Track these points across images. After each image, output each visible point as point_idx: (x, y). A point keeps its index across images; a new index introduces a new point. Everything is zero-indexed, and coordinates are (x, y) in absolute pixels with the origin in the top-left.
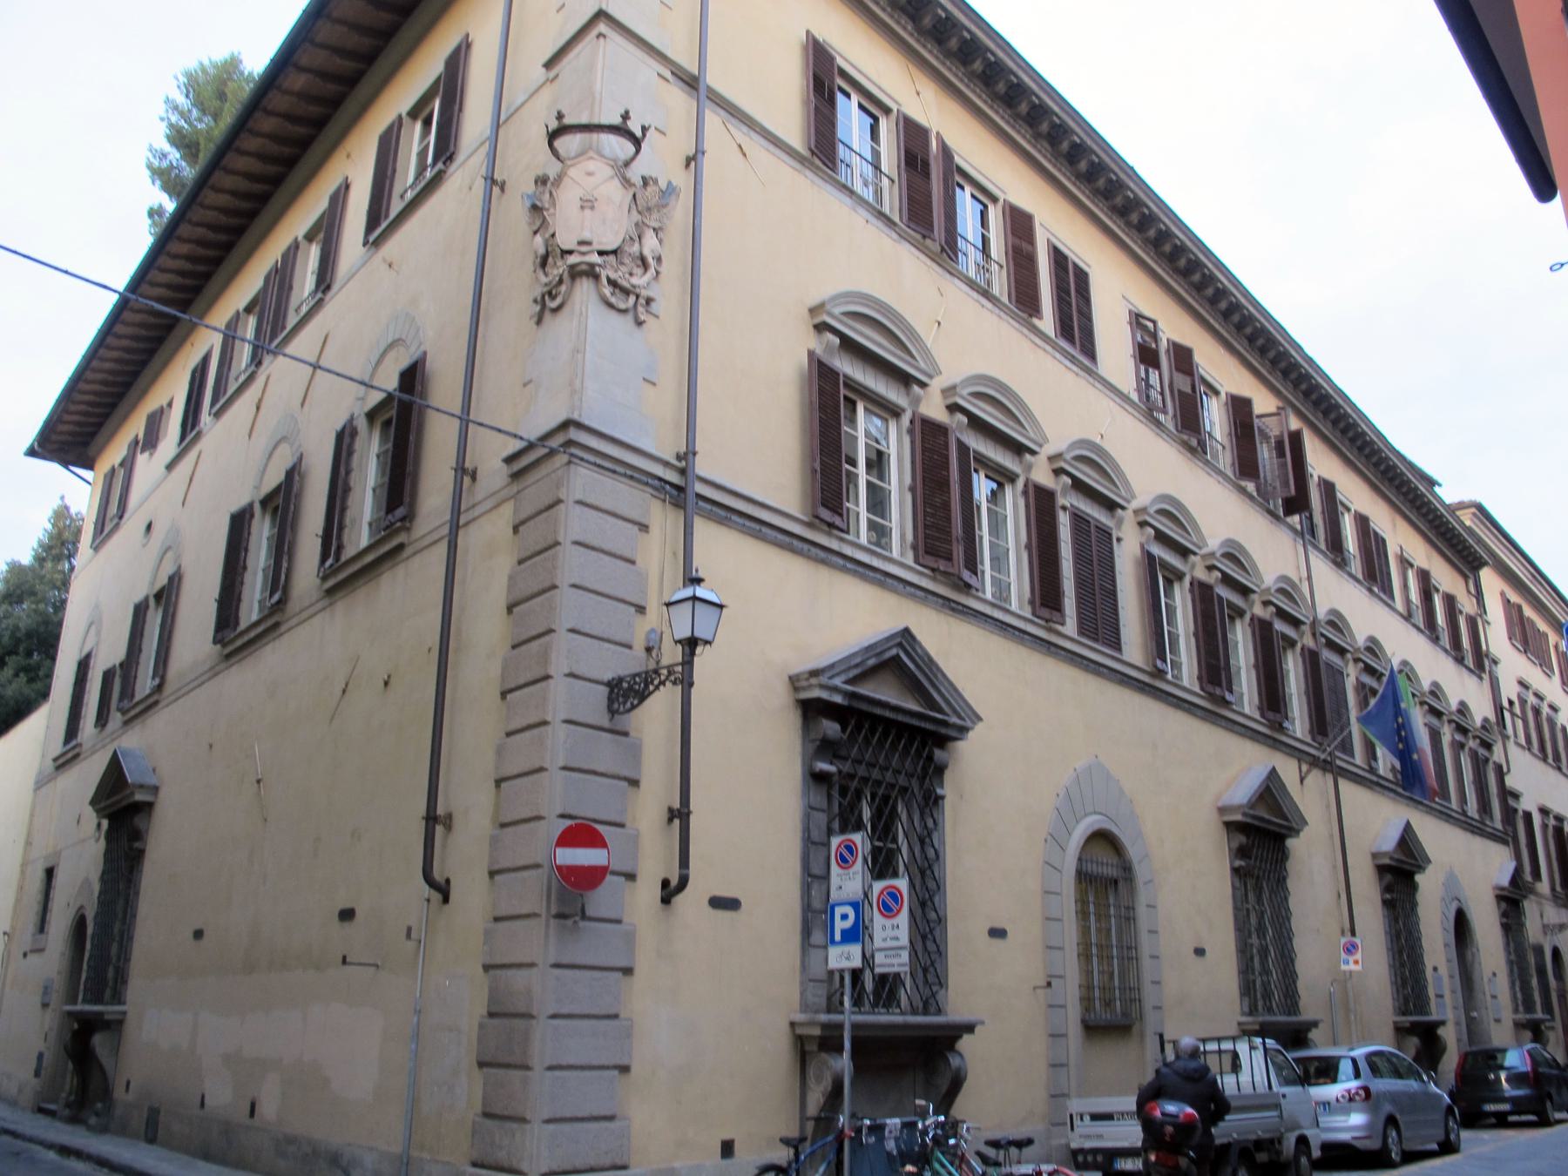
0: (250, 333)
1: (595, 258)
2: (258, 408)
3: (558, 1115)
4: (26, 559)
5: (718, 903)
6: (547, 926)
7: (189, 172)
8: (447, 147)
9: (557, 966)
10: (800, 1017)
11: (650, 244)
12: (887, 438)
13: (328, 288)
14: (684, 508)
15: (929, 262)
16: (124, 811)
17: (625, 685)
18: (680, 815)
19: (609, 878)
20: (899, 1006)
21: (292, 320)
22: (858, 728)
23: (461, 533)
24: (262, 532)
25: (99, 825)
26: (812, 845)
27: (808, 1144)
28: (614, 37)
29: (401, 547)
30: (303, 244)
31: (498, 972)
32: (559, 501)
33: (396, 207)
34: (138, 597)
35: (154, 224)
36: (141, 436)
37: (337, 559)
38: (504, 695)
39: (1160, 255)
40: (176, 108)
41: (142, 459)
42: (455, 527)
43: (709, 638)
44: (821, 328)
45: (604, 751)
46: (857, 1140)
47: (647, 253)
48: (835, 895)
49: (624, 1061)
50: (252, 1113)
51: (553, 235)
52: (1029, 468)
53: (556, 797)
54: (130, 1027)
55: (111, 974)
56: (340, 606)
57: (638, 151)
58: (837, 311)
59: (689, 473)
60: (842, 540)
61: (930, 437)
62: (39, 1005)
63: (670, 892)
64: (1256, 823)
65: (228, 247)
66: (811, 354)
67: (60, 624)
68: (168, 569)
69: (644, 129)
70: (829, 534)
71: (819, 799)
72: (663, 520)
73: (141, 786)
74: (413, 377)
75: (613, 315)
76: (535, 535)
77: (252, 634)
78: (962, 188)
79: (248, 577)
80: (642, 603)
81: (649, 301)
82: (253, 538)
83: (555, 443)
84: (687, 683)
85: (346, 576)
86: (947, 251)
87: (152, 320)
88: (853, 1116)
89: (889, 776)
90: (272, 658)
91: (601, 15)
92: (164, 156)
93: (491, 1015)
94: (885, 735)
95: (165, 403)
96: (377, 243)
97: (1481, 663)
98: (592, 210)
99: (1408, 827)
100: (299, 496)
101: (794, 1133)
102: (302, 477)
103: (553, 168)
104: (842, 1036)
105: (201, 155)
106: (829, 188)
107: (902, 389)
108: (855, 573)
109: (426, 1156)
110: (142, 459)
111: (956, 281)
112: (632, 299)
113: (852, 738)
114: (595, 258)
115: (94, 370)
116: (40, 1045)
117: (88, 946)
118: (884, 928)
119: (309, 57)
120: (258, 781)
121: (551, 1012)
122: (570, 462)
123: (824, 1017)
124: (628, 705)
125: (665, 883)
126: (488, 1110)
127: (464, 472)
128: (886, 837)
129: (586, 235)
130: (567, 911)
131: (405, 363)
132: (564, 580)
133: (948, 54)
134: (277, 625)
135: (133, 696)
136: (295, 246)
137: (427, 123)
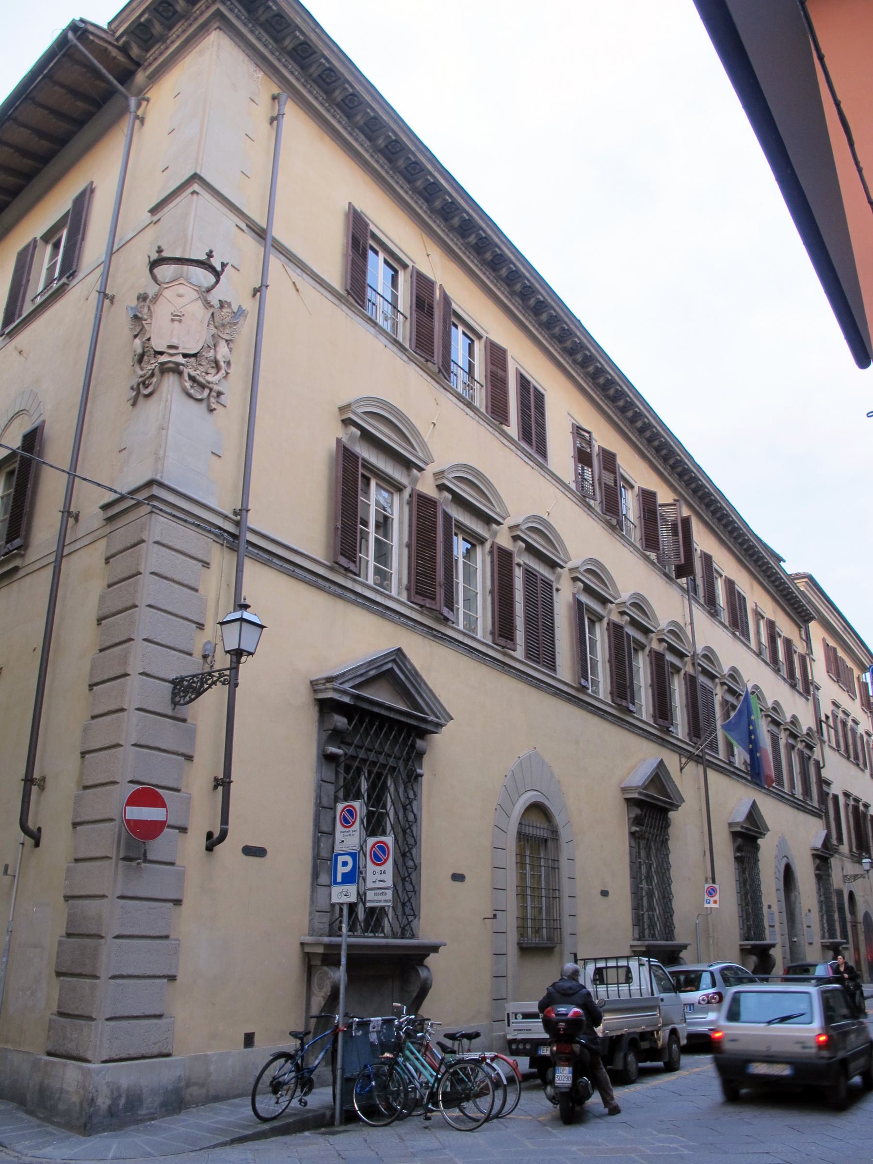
1: (180, 359)
6: (117, 865)
9: (122, 897)
10: (308, 939)
11: (223, 351)
12: (391, 507)
15: (429, 379)
17: (185, 683)
18: (223, 783)
19: (166, 830)
20: (383, 931)
22: (361, 721)
23: (64, 560)
26: (323, 808)
28: (205, 195)
29: (16, 569)
31: (76, 902)
32: (143, 541)
33: (28, 308)
38: (91, 686)
39: (353, 126)
42: (60, 557)
43: (252, 651)
44: (347, 422)
45: (166, 733)
46: (348, 1034)
47: (220, 357)
48: (338, 848)
51: (149, 339)
52: (415, 481)
53: (128, 767)
57: (217, 282)
58: (360, 410)
60: (355, 581)
61: (423, 506)
63: (212, 842)
64: (649, 800)
66: (339, 441)
69: (224, 265)
70: (346, 576)
71: (329, 775)
72: (221, 559)
75: (191, 403)
76: (121, 566)
80: (202, 622)
81: (219, 394)
83: (141, 496)
84: (233, 684)
86: (442, 372)
88: (346, 1015)
91: (196, 177)
93: (69, 935)
97: (807, 688)
98: (180, 322)
99: (754, 805)
101: (301, 1029)
103: (152, 289)
104: (340, 954)
107: (405, 471)
109: (9, 1046)
112: (207, 391)
113: (356, 729)
118: (374, 873)
121: (116, 934)
122: (152, 512)
123: (326, 940)
124: (187, 699)
125: (210, 835)
126: (61, 1010)
127: (69, 515)
129: (174, 342)
130: (132, 855)
131: (28, 428)
132: (143, 602)
137: (56, 246)
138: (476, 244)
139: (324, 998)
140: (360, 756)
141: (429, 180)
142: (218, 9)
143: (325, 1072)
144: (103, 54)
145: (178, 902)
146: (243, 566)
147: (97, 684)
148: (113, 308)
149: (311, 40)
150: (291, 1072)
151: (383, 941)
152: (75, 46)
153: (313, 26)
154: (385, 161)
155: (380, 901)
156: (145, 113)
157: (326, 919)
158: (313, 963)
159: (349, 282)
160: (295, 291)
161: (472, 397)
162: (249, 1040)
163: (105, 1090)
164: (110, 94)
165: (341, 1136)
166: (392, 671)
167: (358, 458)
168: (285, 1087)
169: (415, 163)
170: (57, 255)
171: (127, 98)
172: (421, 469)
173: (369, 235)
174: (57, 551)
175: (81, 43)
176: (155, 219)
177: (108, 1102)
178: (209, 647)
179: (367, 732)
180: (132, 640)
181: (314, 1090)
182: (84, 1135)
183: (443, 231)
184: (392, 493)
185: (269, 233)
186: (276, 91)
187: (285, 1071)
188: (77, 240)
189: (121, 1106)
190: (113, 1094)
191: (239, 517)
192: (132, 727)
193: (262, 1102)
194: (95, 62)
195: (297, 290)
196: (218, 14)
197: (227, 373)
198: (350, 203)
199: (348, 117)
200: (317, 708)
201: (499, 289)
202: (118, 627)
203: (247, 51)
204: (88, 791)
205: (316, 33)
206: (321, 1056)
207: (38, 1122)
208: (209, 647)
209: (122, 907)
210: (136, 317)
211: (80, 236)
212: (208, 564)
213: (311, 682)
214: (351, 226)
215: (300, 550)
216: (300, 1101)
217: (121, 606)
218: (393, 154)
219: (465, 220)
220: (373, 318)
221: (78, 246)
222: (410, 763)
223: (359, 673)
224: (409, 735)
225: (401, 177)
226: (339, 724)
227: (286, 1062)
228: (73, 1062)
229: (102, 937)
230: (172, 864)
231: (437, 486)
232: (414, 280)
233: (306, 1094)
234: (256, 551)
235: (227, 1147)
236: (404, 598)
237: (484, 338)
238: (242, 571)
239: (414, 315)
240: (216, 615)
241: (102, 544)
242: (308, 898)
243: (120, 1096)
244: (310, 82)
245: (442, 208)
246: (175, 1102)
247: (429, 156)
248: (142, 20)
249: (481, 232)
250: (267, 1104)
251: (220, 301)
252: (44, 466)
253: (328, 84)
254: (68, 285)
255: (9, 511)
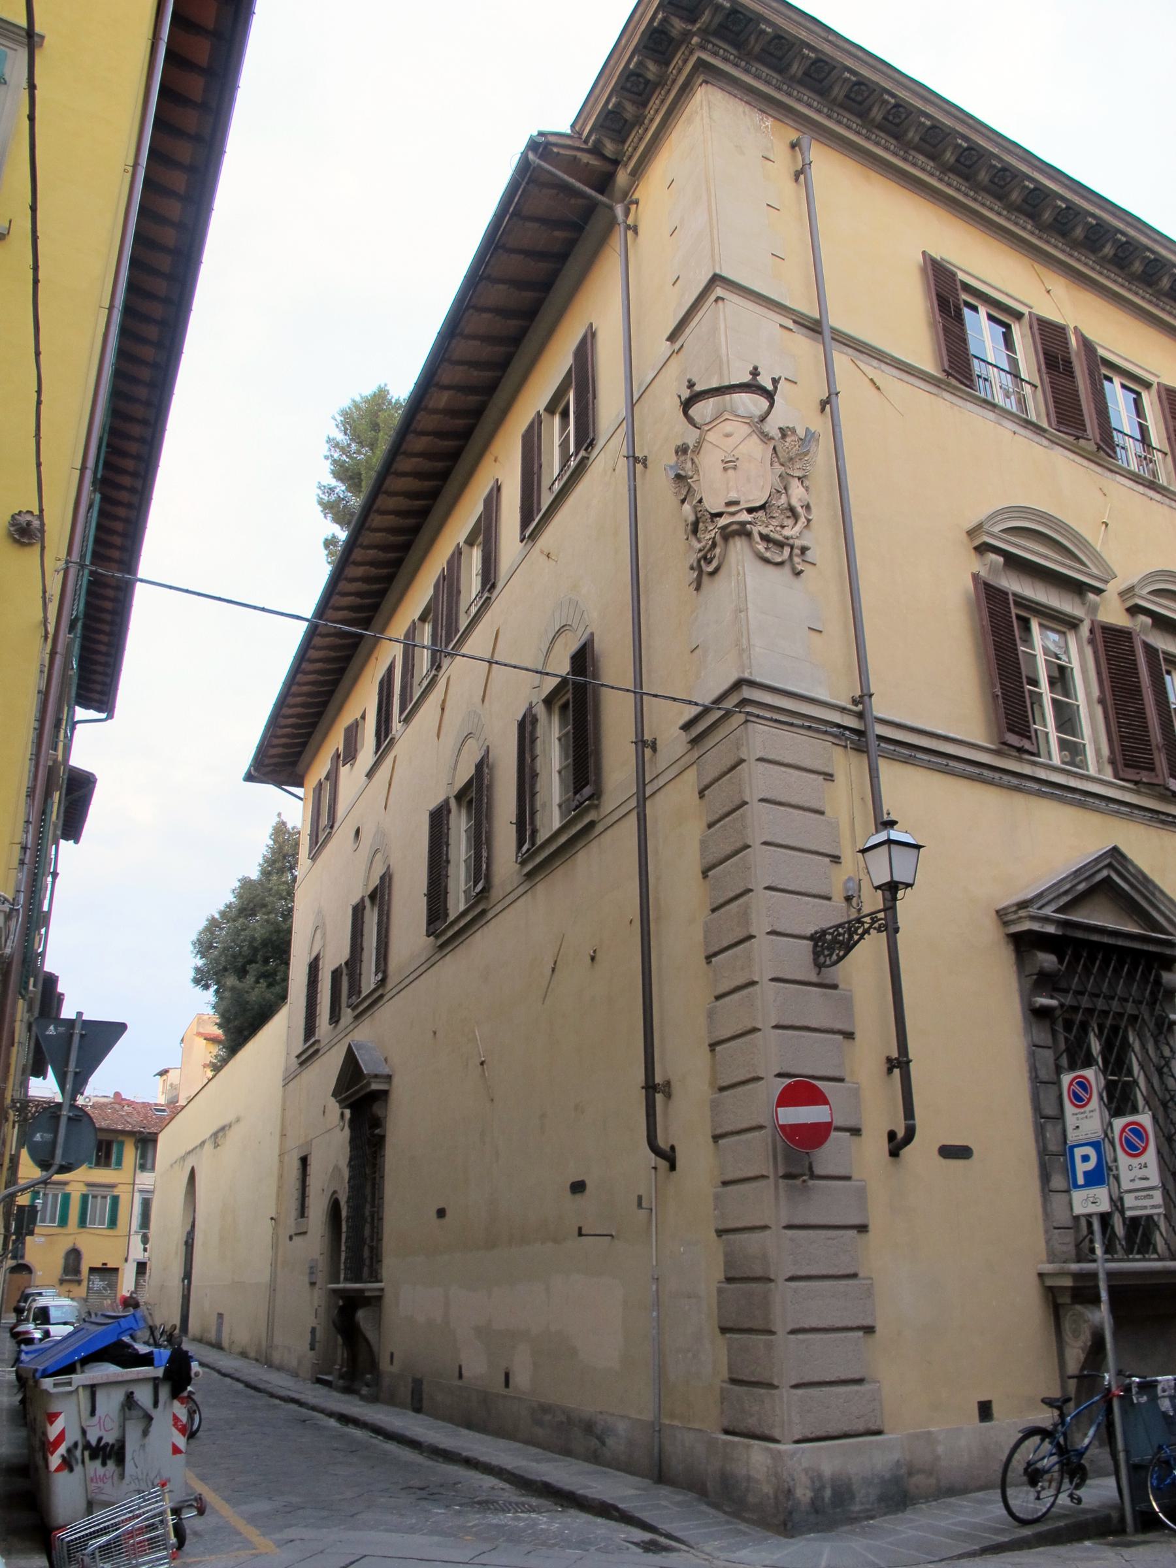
0: (427, 640)
1: (745, 517)
2: (443, 709)
3: (806, 1380)
4: (254, 874)
5: (950, 1152)
6: (776, 1187)
7: (355, 502)
8: (587, 434)
10: (1048, 1268)
11: (797, 493)
12: (1067, 652)
13: (493, 586)
14: (867, 752)
15: (1085, 463)
16: (363, 1102)
17: (829, 937)
18: (899, 1064)
19: (834, 1134)
20: (1155, 1251)
21: (463, 623)
22: (1076, 957)
23: (648, 803)
24: (460, 825)
25: (342, 1115)
26: (1042, 1085)
27: (1072, 1404)
28: (732, 298)
29: (592, 824)
30: (465, 549)
31: (731, 1237)
32: (742, 761)
33: (546, 500)
34: (355, 900)
35: (330, 554)
36: (341, 750)
37: (533, 843)
38: (709, 958)
39: (905, 146)
40: (337, 445)
41: (344, 770)
42: (642, 800)
43: (911, 882)
44: (983, 549)
45: (814, 1007)
46: (1126, 1400)
47: (795, 502)
48: (1072, 1136)
49: (868, 1322)
50: (507, 1384)
51: (700, 501)
52: (1094, 609)
53: (773, 1056)
54: (388, 1300)
55: (366, 1253)
56: (540, 888)
57: (772, 405)
58: (996, 529)
59: (867, 715)
60: (1034, 763)
61: (1113, 645)
62: (308, 1285)
63: (897, 1144)
65: (398, 563)
66: (975, 577)
67: (289, 931)
68: (378, 871)
69: (775, 381)
70: (1021, 760)
71: (1044, 1037)
72: (847, 766)
73: (376, 1076)
74: (583, 659)
75: (770, 569)
76: (720, 797)
77: (462, 923)
78: (1110, 380)
79: (452, 870)
80: (837, 853)
81: (804, 550)
82: (452, 833)
83: (729, 704)
84: (891, 928)
85: (543, 859)
86: (1103, 448)
87: (338, 641)
88: (1120, 1373)
89: (1115, 1004)
90: (483, 944)
91: (716, 279)
92: (332, 490)
93: (729, 1280)
94: (1106, 962)
95: (358, 716)
96: (533, 537)
98: (736, 469)
100: (490, 787)
101: (1056, 1393)
102: (491, 768)
103: (691, 437)
104: (1097, 1287)
105: (363, 484)
106: (969, 405)
107: (1077, 600)
108: (1052, 797)
109: (676, 1423)
110: (344, 770)
111: (1118, 478)
112: (787, 551)
113: (1071, 969)
114: (745, 517)
115: (295, 695)
116: (311, 1321)
117: (344, 1228)
118: (1131, 1168)
119: (448, 376)
120: (482, 1063)
121: (789, 1274)
122: (747, 721)
123: (1074, 1267)
124: (834, 957)
125: (892, 1135)
126: (734, 1376)
127: (645, 745)
128: (1121, 1069)
129: (733, 496)
130: (794, 1171)
131: (574, 647)
132: (755, 840)
133: (1075, 245)
134: (483, 912)
135: (360, 992)
136: (458, 552)
137: (565, 415)
138: (1115, 255)
139: (1083, 1350)
140: (1099, 1008)
141: (1027, 187)
142: (699, 59)
143: (1098, 1455)
144: (572, 166)
145: (862, 1228)
146: (877, 770)
147: (715, 954)
148: (648, 471)
149: (825, 54)
150: (1052, 1455)
151: (1158, 1265)
152: (539, 166)
153: (824, 34)
154: (960, 180)
155: (1145, 1208)
156: (636, 219)
157: (1069, 1238)
158: (1060, 1301)
159: (946, 358)
160: (876, 391)
161: (1154, 474)
162: (985, 1411)
163: (804, 1479)
164: (591, 208)
165: (1141, 1549)
166: (1110, 880)
167: (1006, 594)
168: (1047, 1477)
169: (1004, 169)
170: (568, 425)
171: (611, 208)
172: (1099, 591)
173: (959, 287)
174: (638, 792)
175: (545, 161)
176: (677, 346)
177: (809, 1494)
178: (851, 884)
179: (1087, 971)
180: (751, 890)
181: (1088, 1482)
182: (786, 1536)
183: (1063, 251)
184: (1064, 633)
185: (824, 323)
186: (794, 136)
187: (1043, 1454)
188: (587, 403)
189: (827, 1500)
190: (813, 1482)
191: (860, 707)
192: (769, 1003)
193: (1016, 1498)
194: (566, 177)
195: (878, 388)
196: (701, 65)
197: (809, 521)
198: (924, 253)
199: (896, 138)
200: (1011, 947)
201: (1163, 309)
202: (730, 878)
203: (746, 98)
204: (725, 1093)
205: (829, 41)
206: (1091, 1432)
207: (726, 1517)
208: (851, 884)
209: (792, 1240)
210: (679, 477)
211: (590, 395)
212: (831, 775)
213: (997, 912)
214: (932, 282)
215: (951, 735)
216: (1071, 1496)
217: (729, 849)
218: (969, 167)
219: (1093, 226)
220: (989, 398)
221: (591, 407)
222: (1158, 1007)
223: (1062, 890)
224: (1148, 969)
225: (986, 196)
226: (1046, 965)
227: (1043, 1440)
228: (756, 1442)
229: (771, 1280)
230: (848, 1178)
231: (1128, 610)
232: (1037, 332)
233: (1078, 1487)
234: (892, 748)
235: (977, 1559)
236: (1108, 776)
237: (1155, 385)
238: (878, 777)
239: (1046, 379)
240: (854, 842)
241: (691, 776)
242: (1040, 1210)
243: (823, 1488)
244: (835, 109)
245: (1055, 219)
246: (898, 1495)
247: (1021, 153)
248: (610, 107)
249: (1119, 236)
250: (1024, 1500)
251: (780, 429)
252: (604, 689)
253: (860, 103)
254: (588, 458)
255: (571, 752)
